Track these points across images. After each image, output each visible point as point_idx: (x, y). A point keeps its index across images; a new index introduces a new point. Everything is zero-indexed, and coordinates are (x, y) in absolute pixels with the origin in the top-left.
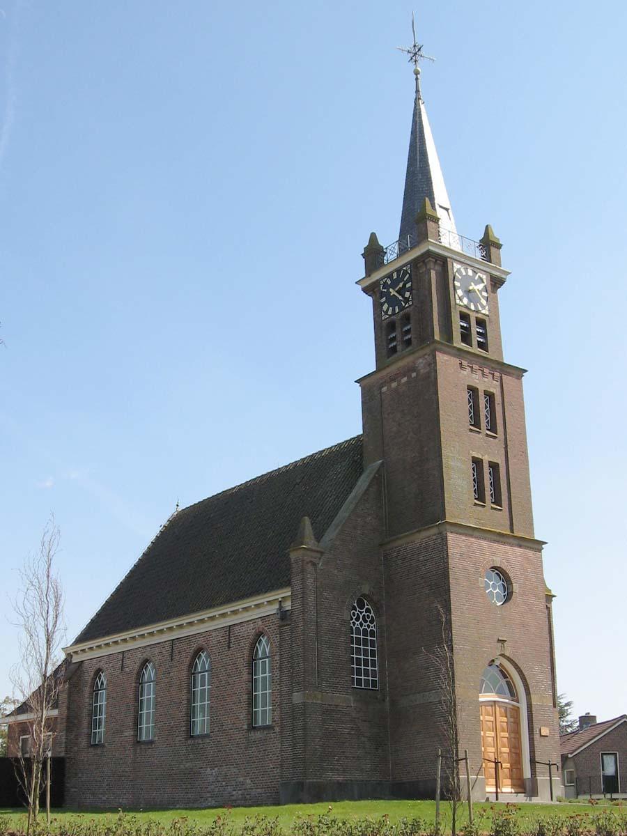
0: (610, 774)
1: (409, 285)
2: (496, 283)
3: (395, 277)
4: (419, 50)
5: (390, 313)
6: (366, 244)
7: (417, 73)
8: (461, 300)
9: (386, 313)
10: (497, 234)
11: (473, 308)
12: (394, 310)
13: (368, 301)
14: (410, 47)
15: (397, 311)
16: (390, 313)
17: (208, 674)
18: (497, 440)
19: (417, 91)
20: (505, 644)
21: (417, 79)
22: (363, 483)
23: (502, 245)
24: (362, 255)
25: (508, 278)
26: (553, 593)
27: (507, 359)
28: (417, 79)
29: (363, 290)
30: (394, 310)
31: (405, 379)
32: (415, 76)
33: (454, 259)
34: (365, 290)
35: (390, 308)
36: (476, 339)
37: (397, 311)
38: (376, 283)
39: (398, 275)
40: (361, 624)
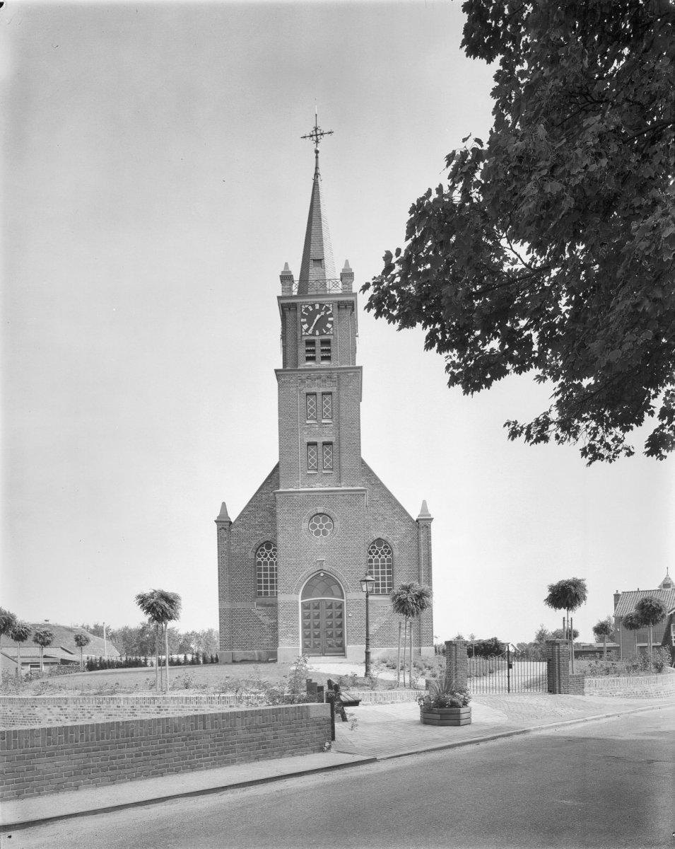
5: (310, 332)
7: (317, 152)
9: (307, 331)
21: (317, 157)
26: (432, 517)
28: (317, 157)
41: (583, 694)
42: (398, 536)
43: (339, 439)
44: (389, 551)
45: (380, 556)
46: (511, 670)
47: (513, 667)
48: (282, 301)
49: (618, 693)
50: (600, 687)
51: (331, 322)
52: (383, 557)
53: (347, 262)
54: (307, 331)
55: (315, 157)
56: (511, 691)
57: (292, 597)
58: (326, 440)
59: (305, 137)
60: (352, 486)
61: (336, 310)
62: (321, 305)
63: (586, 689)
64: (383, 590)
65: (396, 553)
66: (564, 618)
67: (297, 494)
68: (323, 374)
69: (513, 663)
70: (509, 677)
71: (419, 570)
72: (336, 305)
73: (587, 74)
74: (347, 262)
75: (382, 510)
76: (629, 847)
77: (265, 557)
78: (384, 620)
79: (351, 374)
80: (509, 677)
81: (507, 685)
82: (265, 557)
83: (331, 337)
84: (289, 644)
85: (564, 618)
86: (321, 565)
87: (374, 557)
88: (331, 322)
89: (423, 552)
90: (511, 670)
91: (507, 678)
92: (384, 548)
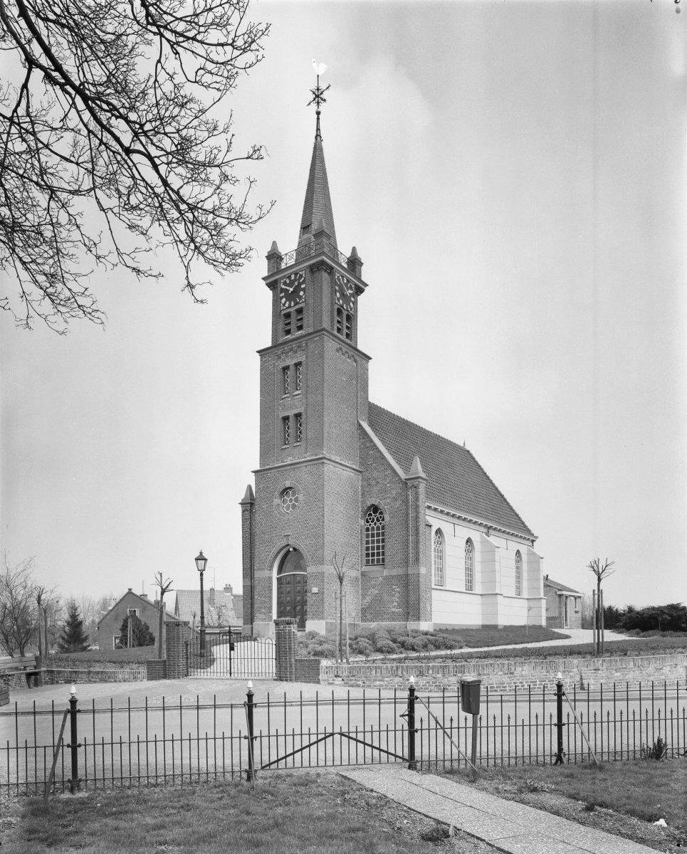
1: (303, 286)
2: (359, 291)
4: (322, 93)
5: (287, 305)
6: (269, 250)
7: (318, 113)
8: (339, 301)
9: (284, 305)
10: (360, 254)
11: (345, 308)
12: (290, 304)
13: (269, 293)
14: (314, 87)
16: (287, 305)
17: (539, 594)
19: (318, 129)
20: (290, 538)
21: (318, 119)
24: (130, 592)
25: (366, 289)
27: (359, 347)
28: (318, 119)
30: (290, 304)
31: (338, 294)
34: (269, 285)
35: (288, 302)
36: (345, 331)
38: (276, 282)
39: (295, 277)
40: (375, 524)
41: (318, 682)
45: (375, 524)
46: (232, 652)
47: (235, 648)
48: (269, 281)
51: (304, 290)
52: (378, 524)
53: (274, 243)
58: (296, 411)
59: (310, 103)
60: (316, 455)
61: (309, 275)
62: (296, 274)
64: (373, 560)
65: (387, 517)
70: (230, 659)
71: (408, 535)
72: (308, 270)
74: (274, 243)
75: (375, 474)
76: (313, 848)
80: (230, 659)
81: (229, 669)
83: (303, 305)
87: (370, 525)
88: (304, 290)
91: (228, 660)
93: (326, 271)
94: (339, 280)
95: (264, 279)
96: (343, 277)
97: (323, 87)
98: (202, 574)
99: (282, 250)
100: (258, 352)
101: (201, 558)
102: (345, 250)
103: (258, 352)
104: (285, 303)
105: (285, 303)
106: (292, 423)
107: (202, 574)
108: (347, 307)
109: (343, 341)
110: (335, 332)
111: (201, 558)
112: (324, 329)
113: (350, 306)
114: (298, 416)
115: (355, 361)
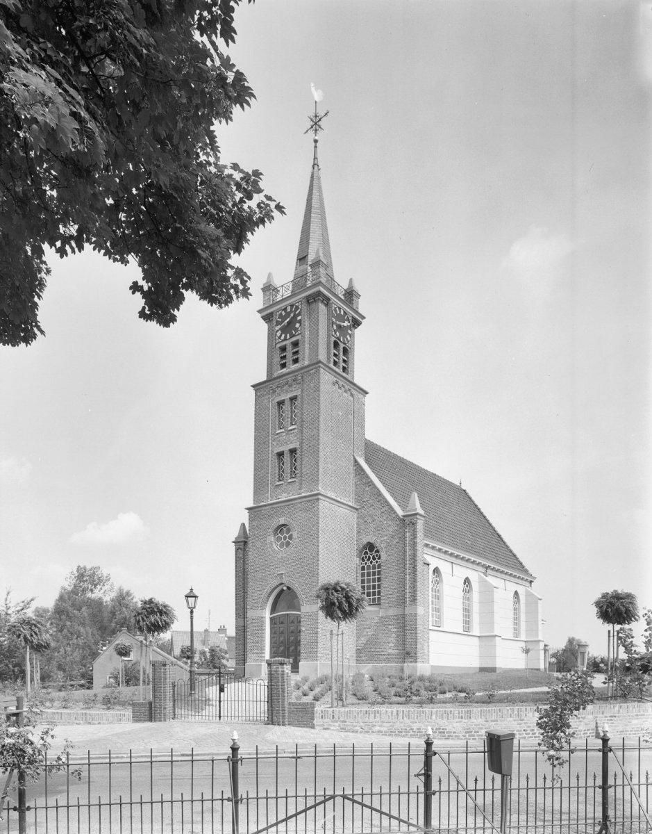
0: (321, 92)
3: (289, 310)
5: (282, 338)
7: (316, 141)
9: (280, 338)
12: (286, 336)
13: (264, 326)
14: (312, 114)
15: (288, 337)
16: (282, 338)
18: (345, 787)
21: (316, 147)
22: (141, 679)
23: (571, 641)
25: (364, 322)
27: (356, 381)
28: (316, 147)
29: (262, 317)
30: (286, 336)
32: (314, 144)
33: (312, 365)
34: (264, 318)
35: (283, 335)
37: (288, 337)
38: (271, 314)
39: (291, 309)
42: (385, 538)
43: (301, 444)
44: (365, 554)
46: (222, 694)
47: (225, 690)
49: (377, 728)
50: (342, 719)
54: (280, 338)
55: (313, 147)
56: (222, 718)
57: (258, 613)
58: (291, 447)
63: (317, 721)
66: (609, 631)
67: (263, 508)
68: (290, 378)
69: (226, 685)
70: (220, 701)
73: (143, 132)
75: (372, 511)
77: (368, 560)
78: (371, 633)
79: (313, 371)
82: (368, 560)
84: (254, 660)
85: (609, 631)
86: (281, 578)
87: (366, 564)
88: (300, 322)
89: (408, 553)
90: (222, 694)
92: (376, 552)
93: (322, 302)
94: (336, 312)
95: (259, 311)
96: (340, 308)
97: (321, 113)
98: (192, 612)
99: (277, 282)
100: (253, 386)
101: (191, 595)
102: (342, 282)
103: (253, 386)
104: (281, 336)
105: (281, 336)
106: (287, 458)
107: (192, 612)
108: (344, 339)
109: (339, 374)
110: (332, 365)
111: (191, 595)
112: (320, 362)
113: (347, 339)
114: (293, 451)
115: (352, 395)
